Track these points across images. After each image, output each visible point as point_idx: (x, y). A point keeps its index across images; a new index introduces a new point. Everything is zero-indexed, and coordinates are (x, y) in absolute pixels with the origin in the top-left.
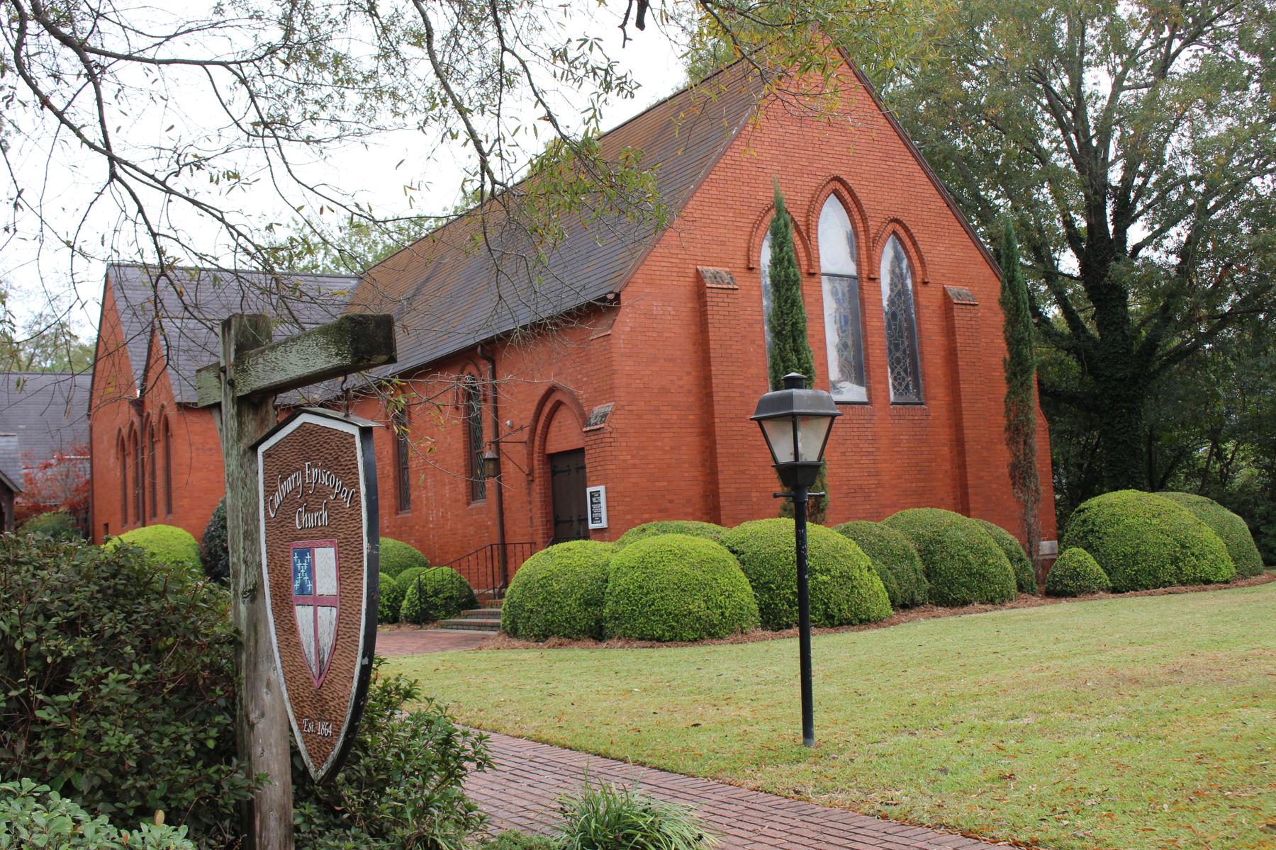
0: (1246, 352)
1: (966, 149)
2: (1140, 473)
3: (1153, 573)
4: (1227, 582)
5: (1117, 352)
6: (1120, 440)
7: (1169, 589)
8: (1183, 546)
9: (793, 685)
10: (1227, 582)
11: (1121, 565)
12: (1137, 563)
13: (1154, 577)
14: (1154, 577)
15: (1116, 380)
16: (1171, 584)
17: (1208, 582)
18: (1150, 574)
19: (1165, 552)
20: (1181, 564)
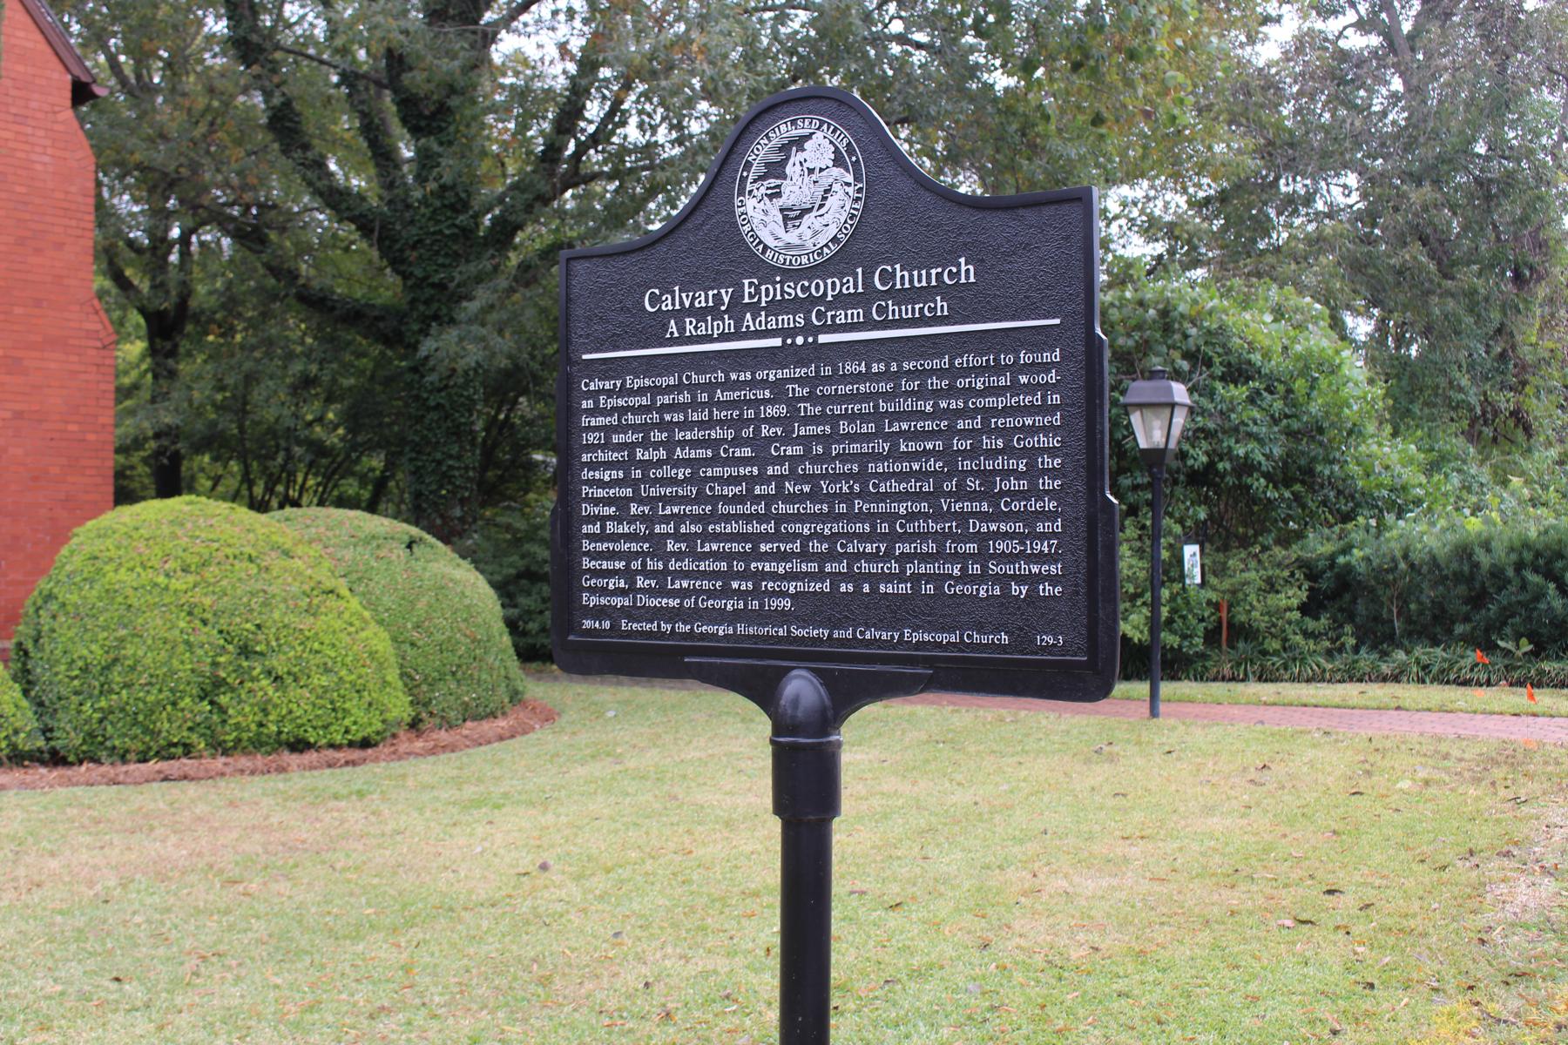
0: (1110, 161)
1: (61, 13)
2: (467, 468)
3: (142, 721)
4: (366, 744)
5: (440, 232)
6: (432, 403)
7: (187, 764)
8: (245, 651)
9: (769, 838)
10: (366, 744)
11: (76, 693)
12: (106, 689)
13: (146, 731)
14: (146, 731)
15: (433, 285)
16: (188, 750)
17: (299, 745)
18: (135, 723)
19: (183, 667)
20: (223, 700)
